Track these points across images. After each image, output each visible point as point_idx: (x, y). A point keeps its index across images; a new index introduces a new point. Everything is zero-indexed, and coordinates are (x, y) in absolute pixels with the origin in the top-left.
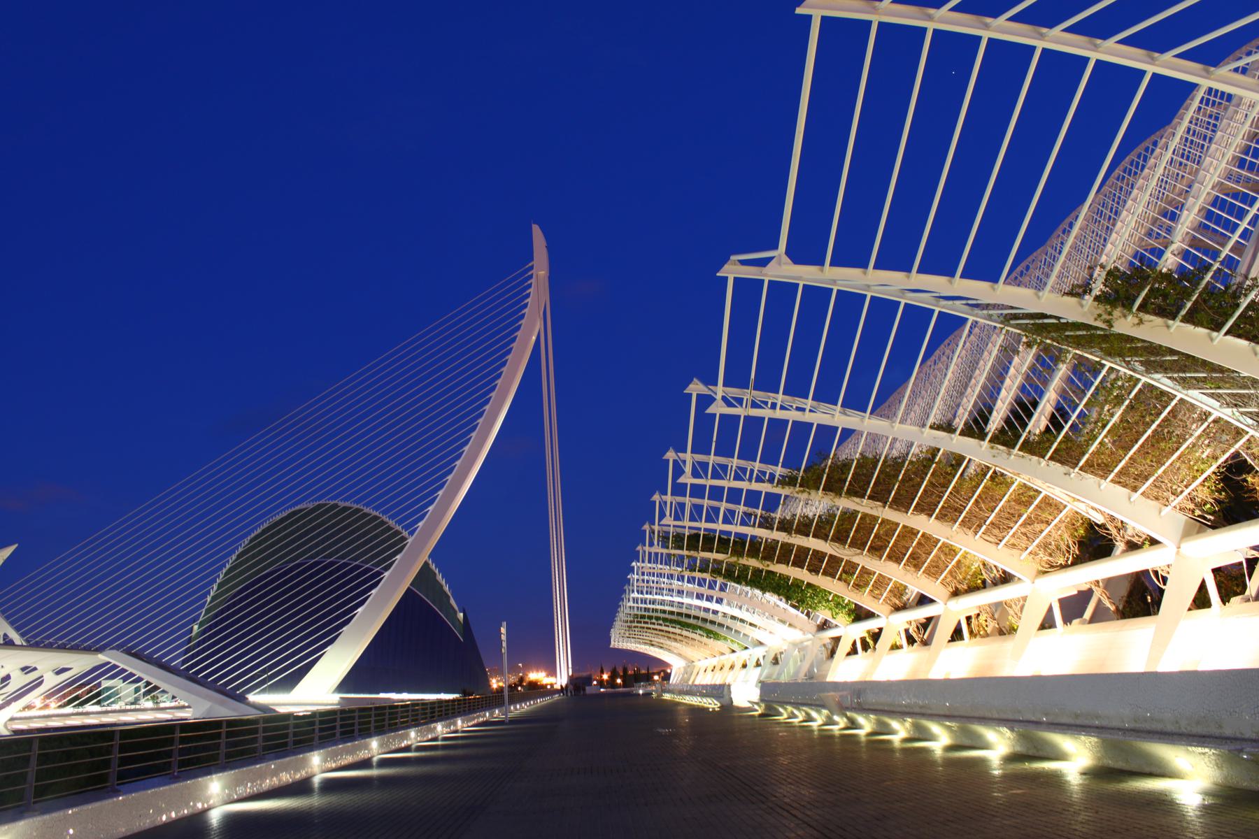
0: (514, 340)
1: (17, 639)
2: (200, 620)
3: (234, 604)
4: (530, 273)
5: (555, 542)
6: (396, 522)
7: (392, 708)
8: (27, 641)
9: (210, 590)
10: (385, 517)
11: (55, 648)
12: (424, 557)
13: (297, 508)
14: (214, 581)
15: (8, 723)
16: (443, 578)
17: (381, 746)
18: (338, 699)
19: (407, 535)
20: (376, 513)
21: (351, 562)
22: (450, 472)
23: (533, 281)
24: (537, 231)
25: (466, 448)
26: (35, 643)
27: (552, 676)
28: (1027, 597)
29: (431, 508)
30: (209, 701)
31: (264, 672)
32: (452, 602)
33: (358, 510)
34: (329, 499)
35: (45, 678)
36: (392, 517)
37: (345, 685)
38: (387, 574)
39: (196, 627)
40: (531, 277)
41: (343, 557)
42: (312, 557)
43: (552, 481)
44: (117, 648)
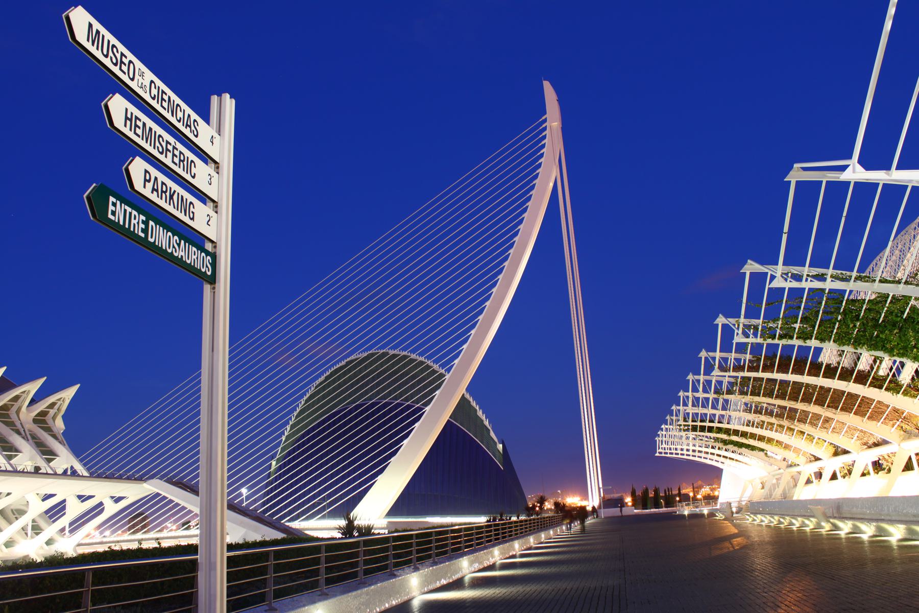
0: (533, 187)
1: (79, 468)
2: (277, 457)
3: (304, 444)
4: (544, 126)
5: (581, 370)
6: (439, 366)
7: (442, 532)
8: (90, 474)
9: (284, 431)
10: (429, 361)
11: (124, 479)
12: (462, 390)
13: (352, 357)
14: (287, 423)
15: (77, 548)
16: (483, 413)
17: (501, 553)
18: (386, 523)
19: (444, 372)
20: (422, 359)
21: (404, 402)
22: (481, 312)
23: (547, 132)
24: (547, 86)
25: (494, 290)
26: (96, 474)
27: (585, 500)
28: (903, 471)
29: (465, 346)
30: (244, 527)
31: (324, 499)
32: (492, 434)
33: (405, 357)
34: (378, 349)
35: (68, 504)
36: (436, 362)
37: (395, 510)
38: (427, 409)
39: (274, 463)
40: (545, 129)
41: (396, 398)
42: (370, 398)
43: (574, 306)
44: (161, 478)
